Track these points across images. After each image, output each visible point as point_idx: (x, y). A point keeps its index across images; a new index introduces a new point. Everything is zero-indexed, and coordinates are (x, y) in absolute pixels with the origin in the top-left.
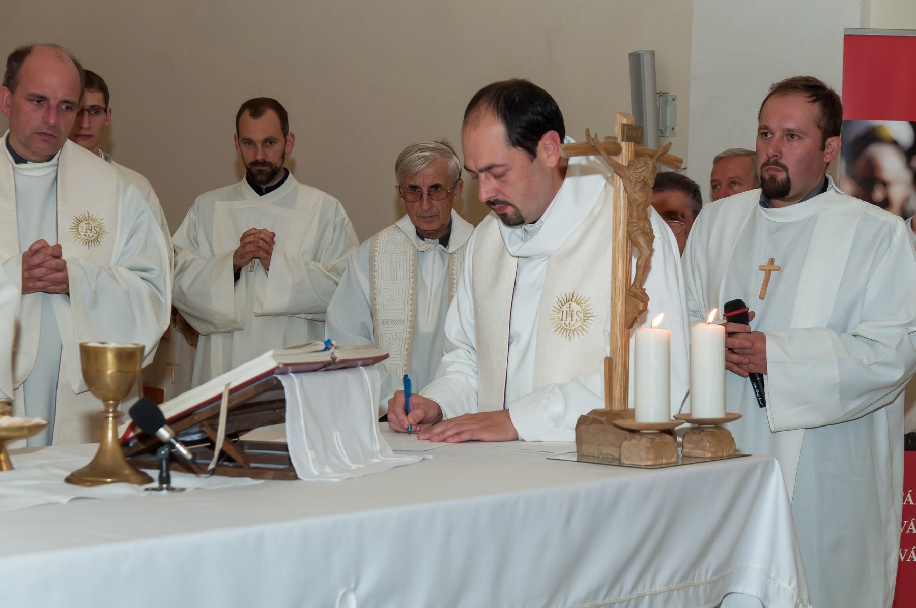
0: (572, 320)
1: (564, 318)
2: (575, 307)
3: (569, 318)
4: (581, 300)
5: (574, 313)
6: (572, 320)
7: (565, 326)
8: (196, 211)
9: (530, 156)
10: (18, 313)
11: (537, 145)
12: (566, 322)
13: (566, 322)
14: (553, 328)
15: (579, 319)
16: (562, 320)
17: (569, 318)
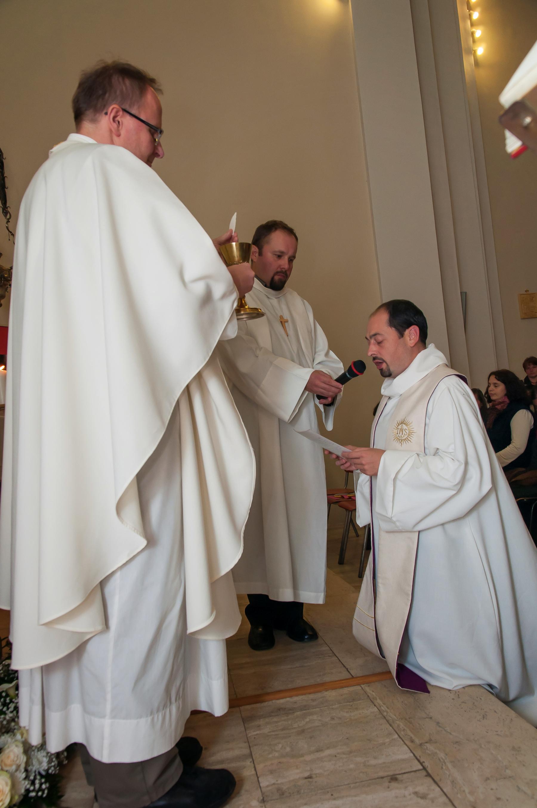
0: (402, 434)
1: (399, 433)
2: (404, 427)
3: (401, 433)
4: (408, 422)
5: (404, 430)
6: (402, 434)
7: (399, 437)
8: (492, 395)
9: (400, 335)
10: (497, 368)
11: (405, 330)
12: (399, 435)
13: (399, 435)
14: (393, 438)
15: (406, 434)
16: (397, 434)
17: (401, 433)
